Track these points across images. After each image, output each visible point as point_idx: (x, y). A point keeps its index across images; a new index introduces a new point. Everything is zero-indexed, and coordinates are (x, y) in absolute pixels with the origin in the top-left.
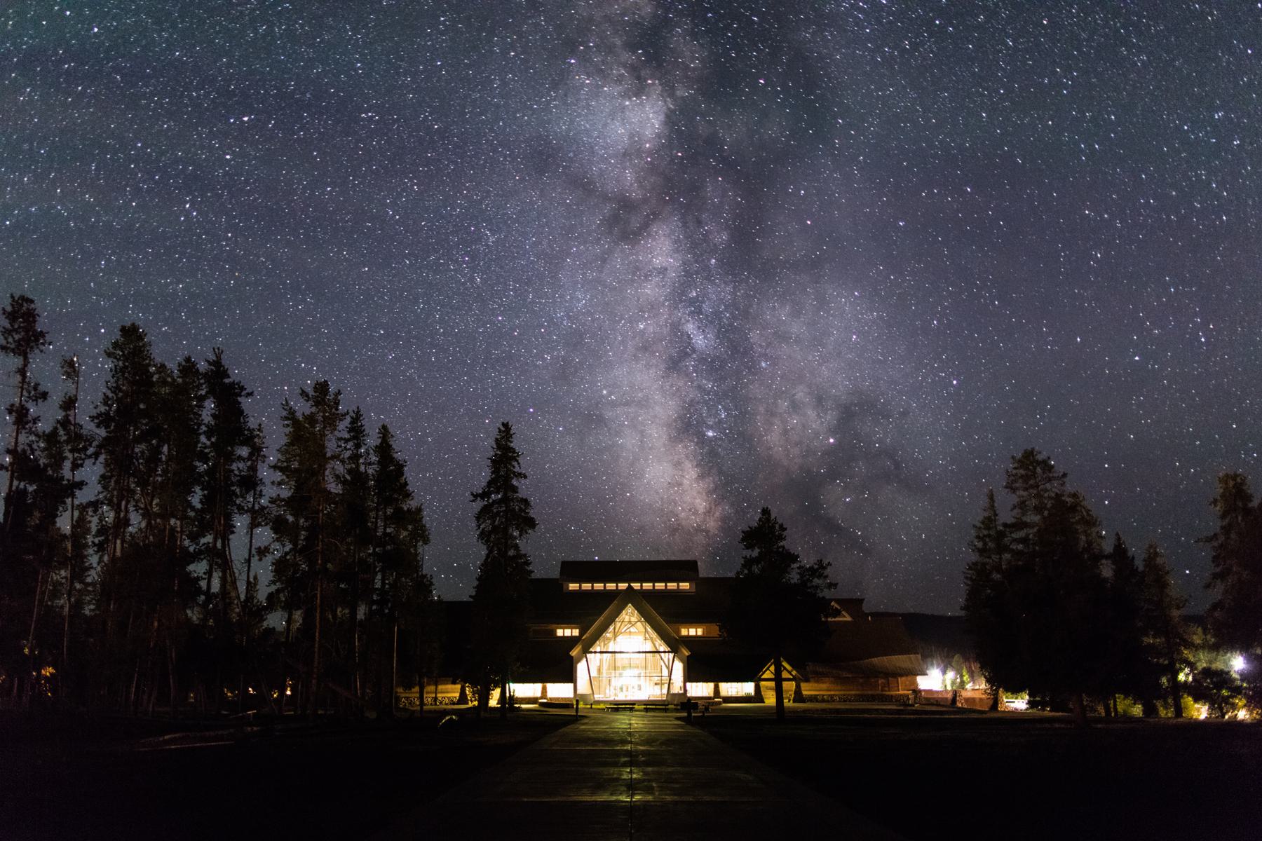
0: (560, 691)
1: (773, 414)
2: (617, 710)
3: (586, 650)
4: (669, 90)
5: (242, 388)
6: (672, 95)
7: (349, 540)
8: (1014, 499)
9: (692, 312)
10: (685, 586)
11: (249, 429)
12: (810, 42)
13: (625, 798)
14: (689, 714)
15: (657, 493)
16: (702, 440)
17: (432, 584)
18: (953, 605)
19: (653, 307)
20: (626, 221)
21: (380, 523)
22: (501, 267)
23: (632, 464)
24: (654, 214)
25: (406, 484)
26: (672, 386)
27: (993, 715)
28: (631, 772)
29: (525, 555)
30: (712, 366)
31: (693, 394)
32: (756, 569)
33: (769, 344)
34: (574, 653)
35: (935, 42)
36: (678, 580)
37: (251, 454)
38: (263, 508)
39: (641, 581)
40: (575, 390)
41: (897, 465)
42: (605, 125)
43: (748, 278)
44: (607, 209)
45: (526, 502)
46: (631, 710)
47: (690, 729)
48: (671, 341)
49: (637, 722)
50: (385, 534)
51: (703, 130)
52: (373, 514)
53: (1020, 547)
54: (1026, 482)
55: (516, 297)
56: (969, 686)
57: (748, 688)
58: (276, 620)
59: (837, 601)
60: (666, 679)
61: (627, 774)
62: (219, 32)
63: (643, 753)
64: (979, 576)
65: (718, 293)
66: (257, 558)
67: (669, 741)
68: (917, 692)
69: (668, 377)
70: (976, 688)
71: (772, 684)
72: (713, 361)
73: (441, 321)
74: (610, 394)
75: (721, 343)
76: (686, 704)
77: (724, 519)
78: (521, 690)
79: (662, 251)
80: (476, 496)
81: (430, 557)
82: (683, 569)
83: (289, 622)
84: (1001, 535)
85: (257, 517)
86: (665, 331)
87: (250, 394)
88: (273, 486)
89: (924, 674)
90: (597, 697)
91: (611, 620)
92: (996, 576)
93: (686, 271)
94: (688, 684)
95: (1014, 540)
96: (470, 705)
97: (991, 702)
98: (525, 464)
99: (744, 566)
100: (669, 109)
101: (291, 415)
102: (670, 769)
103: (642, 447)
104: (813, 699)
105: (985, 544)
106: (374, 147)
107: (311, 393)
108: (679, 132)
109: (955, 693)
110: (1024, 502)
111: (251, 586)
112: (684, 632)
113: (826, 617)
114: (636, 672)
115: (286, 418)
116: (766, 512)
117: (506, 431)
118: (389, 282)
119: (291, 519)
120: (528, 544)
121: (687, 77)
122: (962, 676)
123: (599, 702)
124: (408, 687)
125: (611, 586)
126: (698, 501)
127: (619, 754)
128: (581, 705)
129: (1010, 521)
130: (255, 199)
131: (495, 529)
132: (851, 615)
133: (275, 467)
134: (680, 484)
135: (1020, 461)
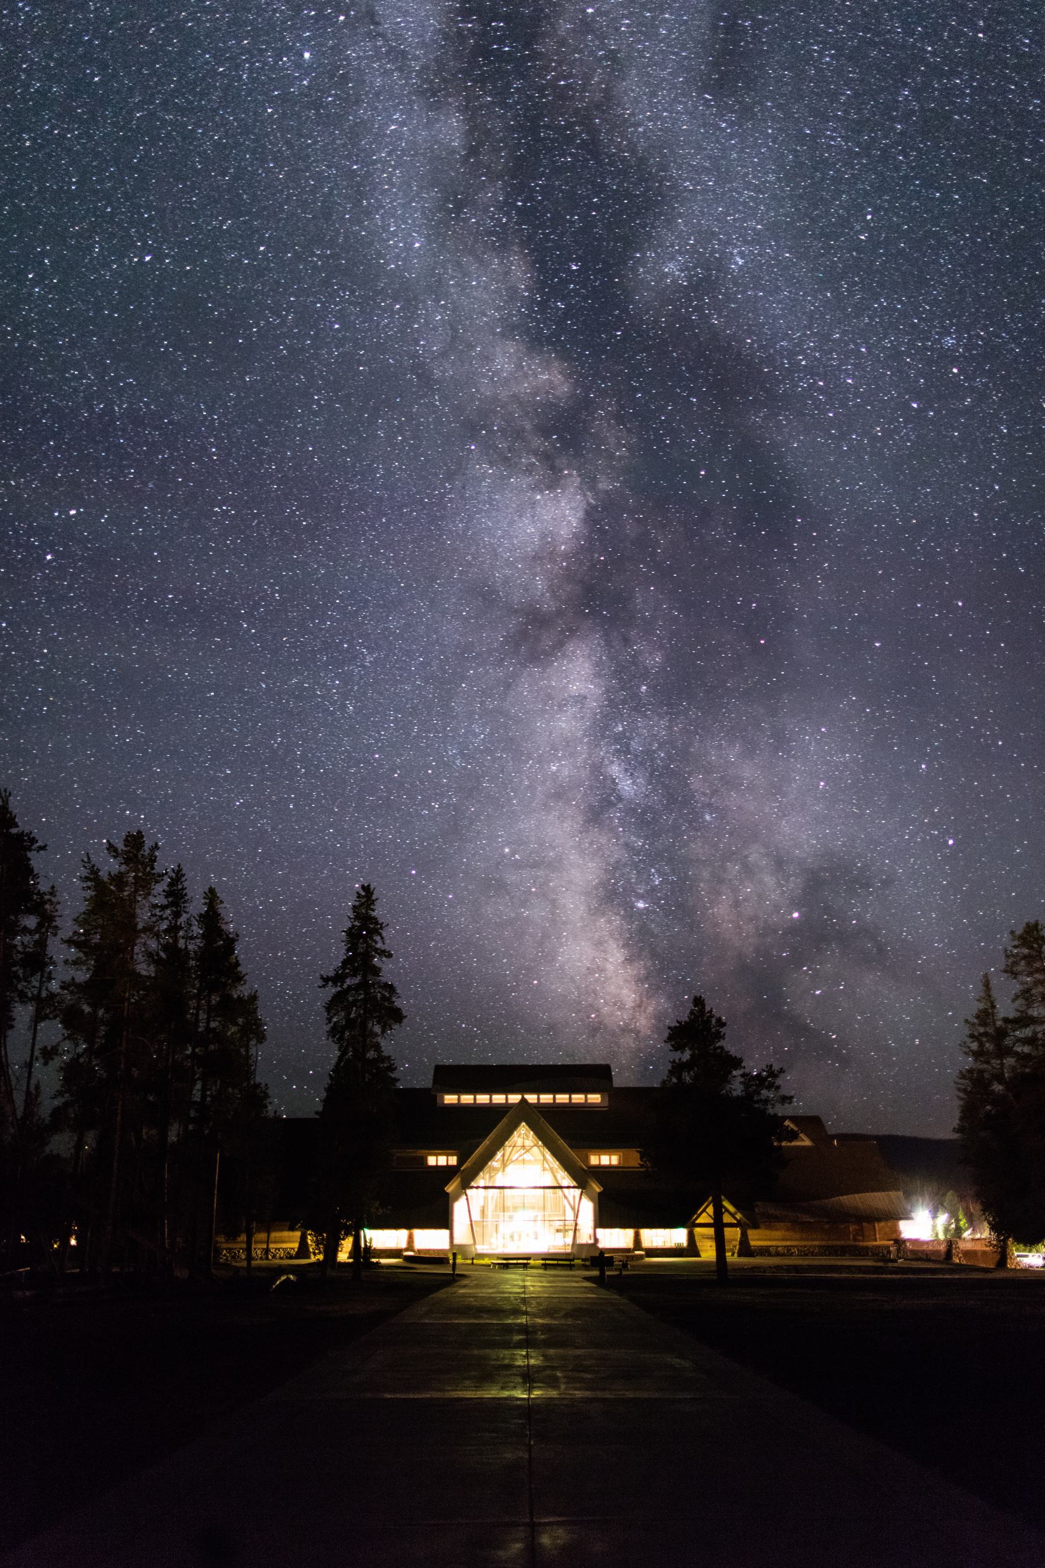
0: (430, 1240)
1: (721, 881)
2: (506, 1266)
3: (466, 1185)
4: (590, 482)
5: (33, 841)
6: (593, 488)
7: (162, 1036)
8: (1015, 987)
9: (617, 751)
10: (595, 1098)
11: (39, 893)
12: (761, 427)
13: (520, 1394)
14: (602, 1272)
15: (572, 979)
16: (630, 913)
17: (267, 1096)
18: (942, 1122)
19: (569, 743)
20: (535, 636)
21: (203, 1016)
22: (381, 694)
23: (541, 943)
24: (570, 630)
25: (237, 964)
26: (591, 843)
27: (1000, 1275)
28: (527, 1357)
29: (389, 1058)
30: (643, 819)
31: (619, 854)
32: (687, 1078)
33: (715, 792)
34: (450, 1188)
35: (913, 429)
36: (586, 1091)
37: (40, 925)
38: (52, 996)
39: (538, 1091)
40: (470, 846)
41: (881, 950)
42: (511, 523)
43: (688, 709)
44: (513, 623)
45: (391, 988)
46: (525, 1266)
47: (604, 1294)
48: (591, 788)
49: (530, 1284)
50: (208, 1029)
51: (630, 529)
52: (193, 1003)
53: (1026, 1049)
54: (1029, 964)
55: (396, 730)
56: (967, 1234)
57: (678, 1237)
58: (61, 1144)
59: (793, 1119)
60: (570, 1225)
61: (521, 1358)
62: (47, 411)
63: (547, 1329)
64: (976, 1088)
65: (652, 729)
66: (41, 1060)
67: (578, 1311)
68: (899, 1242)
69: (587, 832)
70: (978, 1236)
71: (711, 1231)
72: (644, 813)
73: (303, 759)
74: (513, 853)
75: (654, 790)
76: (598, 1259)
77: (658, 1017)
78: (383, 1239)
79: (578, 675)
80: (326, 980)
81: (265, 1059)
82: (592, 1075)
83: (79, 1146)
84: (1001, 1033)
85: (45, 1007)
86: (584, 774)
87: (43, 848)
88: (66, 967)
89: (908, 1217)
90: (481, 1248)
91: (499, 1143)
92: (997, 1087)
93: (610, 700)
94: (599, 1231)
95: (1019, 1040)
96: (313, 1259)
97: (997, 1257)
98: (390, 938)
99: (671, 1072)
100: (589, 504)
101: (93, 876)
102: (579, 1352)
103: (554, 922)
104: (764, 1251)
105: (981, 1045)
106: (228, 546)
107: (120, 846)
108: (602, 532)
109: (950, 1244)
110: (1028, 991)
111: (32, 1099)
112: (594, 1160)
113: (780, 1140)
114: (531, 1214)
115: (87, 879)
116: (698, 1001)
117: (367, 896)
118: (240, 709)
119: (87, 1009)
120: (392, 1043)
121: (613, 468)
122: (958, 1221)
123: (482, 1256)
124: (232, 1236)
125: (499, 1099)
126: (625, 991)
127: (509, 1329)
128: (459, 1261)
129: (1012, 1015)
130: (80, 608)
131: (350, 1024)
132: (812, 1140)
133: (70, 942)
134: (601, 970)
135: (1021, 937)
